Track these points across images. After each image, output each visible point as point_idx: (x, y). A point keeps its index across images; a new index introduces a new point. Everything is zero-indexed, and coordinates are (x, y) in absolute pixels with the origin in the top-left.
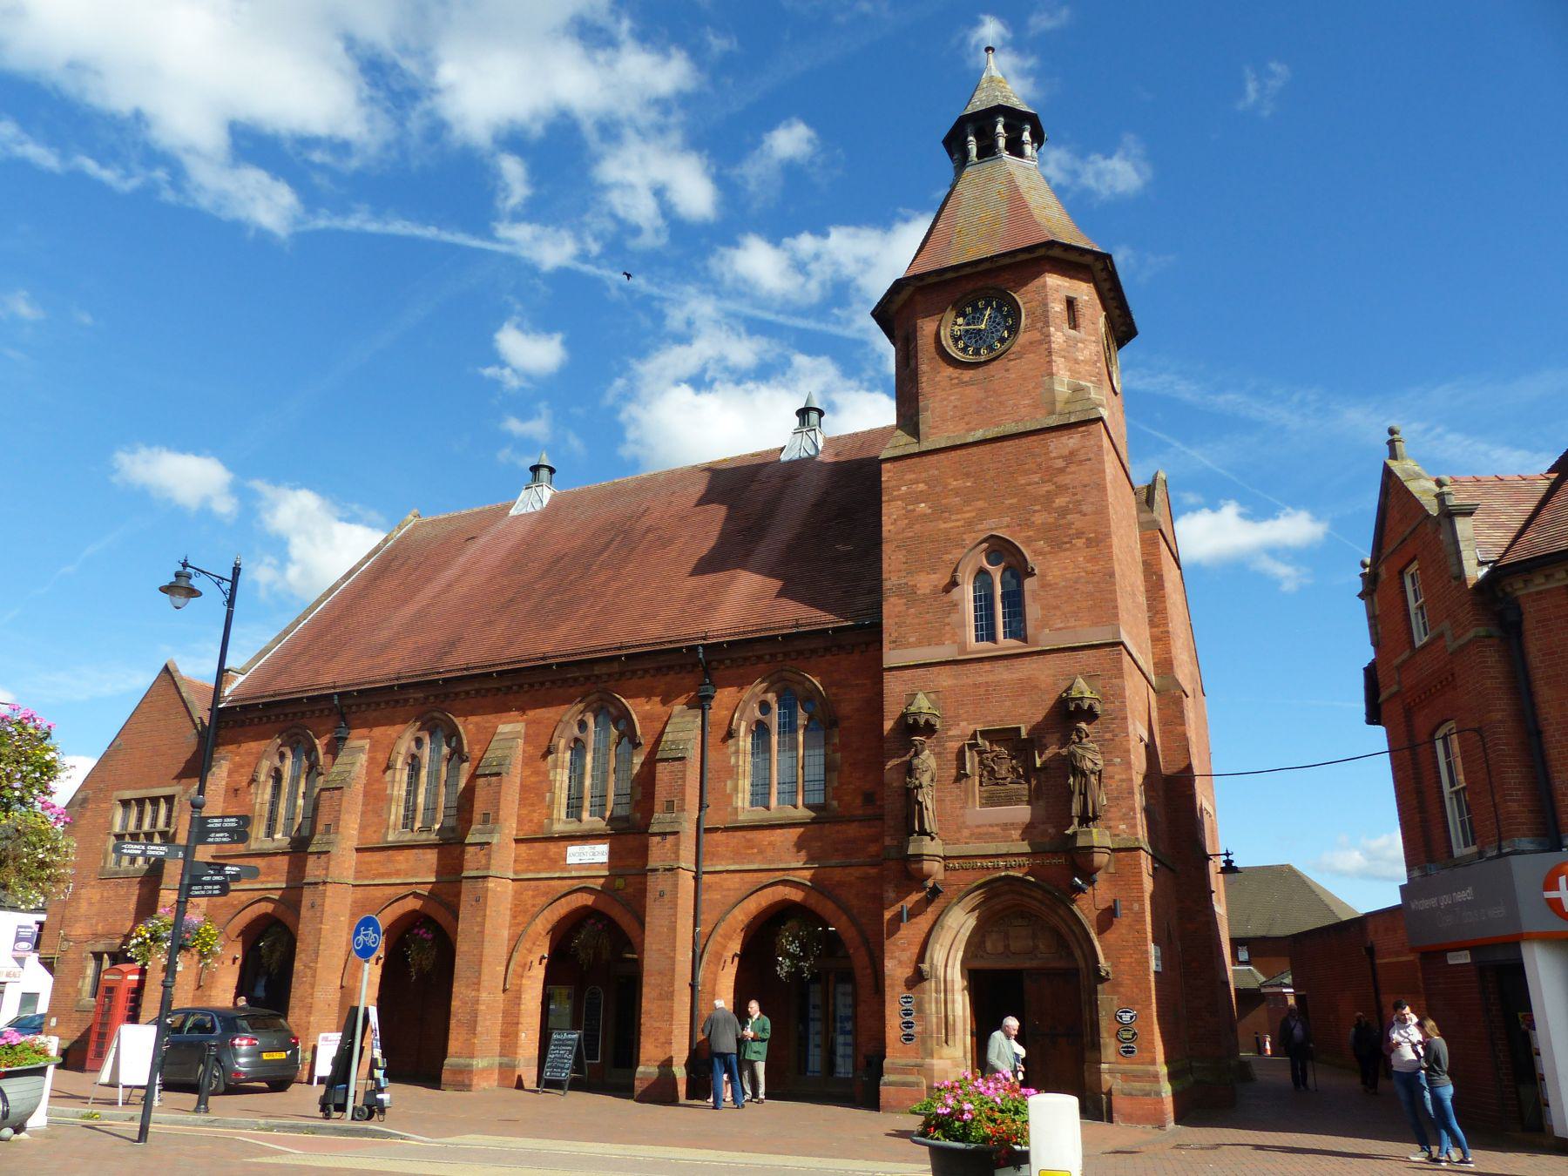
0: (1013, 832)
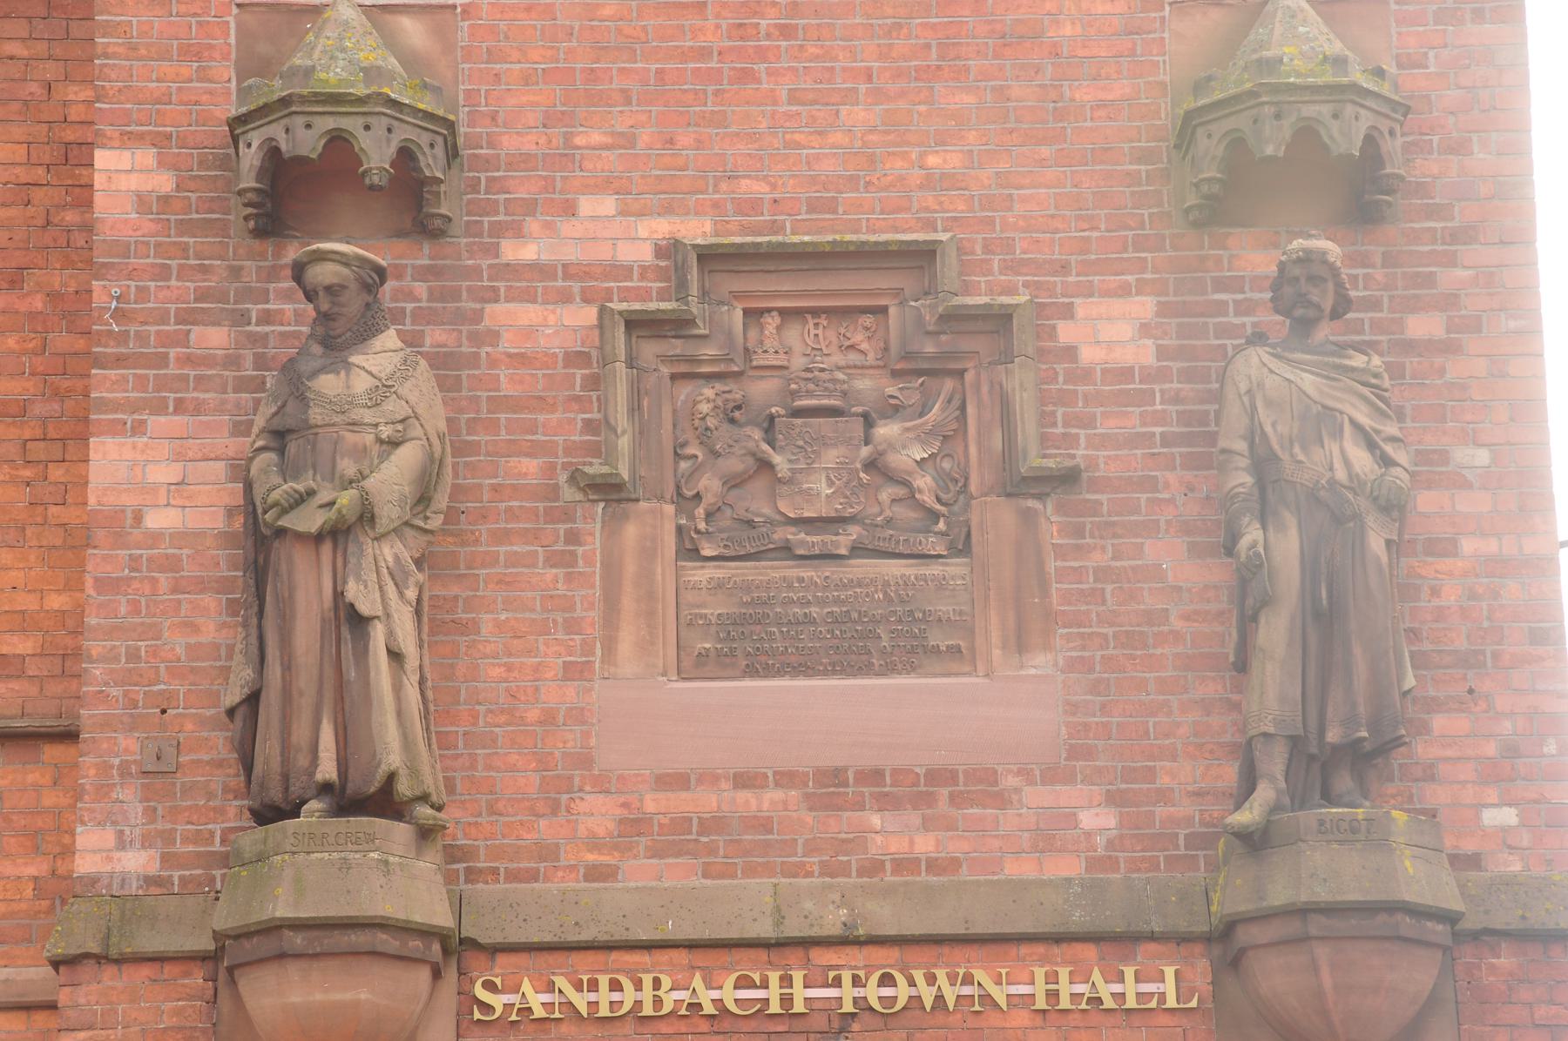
0: (876, 820)
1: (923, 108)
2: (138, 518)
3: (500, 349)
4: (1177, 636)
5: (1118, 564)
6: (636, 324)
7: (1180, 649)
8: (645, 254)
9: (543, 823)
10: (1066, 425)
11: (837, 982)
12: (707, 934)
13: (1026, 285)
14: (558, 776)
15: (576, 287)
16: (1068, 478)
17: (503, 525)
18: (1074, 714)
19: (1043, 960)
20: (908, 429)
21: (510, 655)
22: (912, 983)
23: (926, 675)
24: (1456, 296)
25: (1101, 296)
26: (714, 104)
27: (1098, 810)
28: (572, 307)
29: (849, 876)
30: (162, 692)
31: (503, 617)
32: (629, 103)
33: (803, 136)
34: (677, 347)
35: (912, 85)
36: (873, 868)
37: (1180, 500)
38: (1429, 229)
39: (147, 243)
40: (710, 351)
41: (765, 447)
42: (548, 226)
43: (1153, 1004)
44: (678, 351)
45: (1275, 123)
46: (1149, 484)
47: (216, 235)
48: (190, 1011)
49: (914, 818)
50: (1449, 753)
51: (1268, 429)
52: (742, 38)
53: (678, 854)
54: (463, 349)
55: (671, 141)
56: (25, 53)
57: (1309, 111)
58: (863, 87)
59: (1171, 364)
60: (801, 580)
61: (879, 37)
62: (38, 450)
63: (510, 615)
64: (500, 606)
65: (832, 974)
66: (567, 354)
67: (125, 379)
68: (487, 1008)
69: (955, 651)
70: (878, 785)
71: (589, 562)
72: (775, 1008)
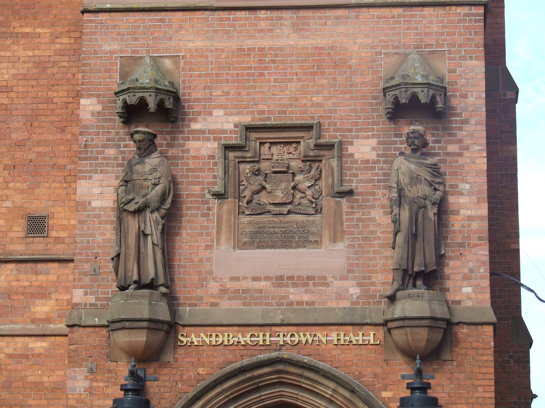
0: (292, 290)
1: (312, 84)
2: (90, 203)
3: (190, 155)
4: (379, 238)
5: (363, 217)
6: (228, 148)
7: (380, 242)
8: (231, 127)
9: (198, 290)
10: (350, 176)
11: (279, 336)
12: (243, 322)
13: (340, 135)
14: (203, 277)
15: (212, 136)
16: (350, 193)
17: (189, 205)
18: (349, 260)
19: (337, 330)
20: (305, 177)
21: (190, 242)
22: (300, 337)
23: (308, 249)
24: (462, 140)
25: (362, 138)
26: (252, 83)
27: (354, 288)
28: (211, 142)
29: (284, 306)
30: (95, 252)
31: (189, 232)
32: (228, 83)
33: (277, 92)
34: (239, 154)
35: (309, 77)
36: (291, 304)
37: (382, 198)
38: (455, 120)
39: (94, 125)
40: (249, 155)
41: (264, 182)
42: (204, 119)
43: (367, 343)
44: (240, 155)
45: (405, 93)
46: (373, 194)
47: (112, 123)
48: (102, 341)
49: (303, 289)
50: (454, 272)
51: (402, 181)
52: (261, 64)
53: (236, 299)
54: (179, 155)
55: (240, 94)
56: (68, 65)
57: (415, 90)
58: (295, 78)
59: (380, 159)
60: (273, 221)
61: (300, 63)
62: (69, 179)
63: (190, 231)
64: (188, 228)
65: (277, 334)
66: (208, 156)
67: (87, 164)
68: (182, 342)
69: (316, 242)
70: (293, 280)
71: (213, 216)
72: (261, 343)
